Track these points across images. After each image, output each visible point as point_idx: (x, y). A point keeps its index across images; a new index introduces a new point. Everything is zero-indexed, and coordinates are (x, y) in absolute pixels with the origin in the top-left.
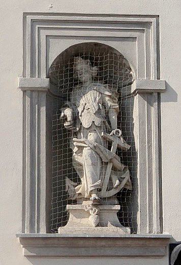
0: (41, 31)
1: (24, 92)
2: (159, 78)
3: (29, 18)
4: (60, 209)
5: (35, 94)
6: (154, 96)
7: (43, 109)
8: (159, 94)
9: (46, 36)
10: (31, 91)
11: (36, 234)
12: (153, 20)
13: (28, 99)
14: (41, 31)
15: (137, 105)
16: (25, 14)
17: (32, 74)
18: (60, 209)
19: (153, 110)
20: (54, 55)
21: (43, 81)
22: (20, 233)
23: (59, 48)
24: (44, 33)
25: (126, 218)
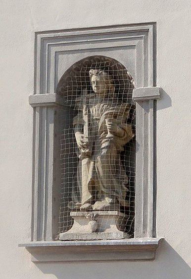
0: (60, 56)
1: (35, 108)
2: (155, 85)
3: (151, 27)
4: (66, 214)
5: (45, 110)
6: (154, 102)
7: (52, 127)
8: (155, 101)
9: (56, 52)
10: (40, 107)
11: (43, 242)
12: (151, 27)
13: (37, 114)
14: (60, 56)
15: (139, 110)
16: (36, 33)
17: (42, 92)
18: (66, 214)
19: (150, 114)
20: (63, 68)
21: (51, 96)
22: (28, 241)
23: (67, 62)
24: (54, 49)
25: (128, 228)
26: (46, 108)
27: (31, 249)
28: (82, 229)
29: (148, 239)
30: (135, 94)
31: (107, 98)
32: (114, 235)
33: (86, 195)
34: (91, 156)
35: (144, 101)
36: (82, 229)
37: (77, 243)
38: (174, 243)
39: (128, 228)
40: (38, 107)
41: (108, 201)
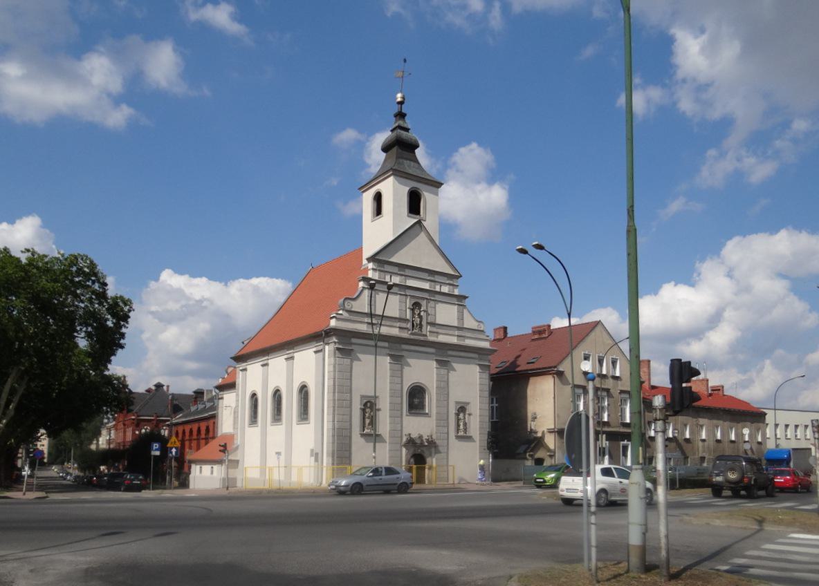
6: (379, 410)
28: (366, 431)
36: (366, 431)
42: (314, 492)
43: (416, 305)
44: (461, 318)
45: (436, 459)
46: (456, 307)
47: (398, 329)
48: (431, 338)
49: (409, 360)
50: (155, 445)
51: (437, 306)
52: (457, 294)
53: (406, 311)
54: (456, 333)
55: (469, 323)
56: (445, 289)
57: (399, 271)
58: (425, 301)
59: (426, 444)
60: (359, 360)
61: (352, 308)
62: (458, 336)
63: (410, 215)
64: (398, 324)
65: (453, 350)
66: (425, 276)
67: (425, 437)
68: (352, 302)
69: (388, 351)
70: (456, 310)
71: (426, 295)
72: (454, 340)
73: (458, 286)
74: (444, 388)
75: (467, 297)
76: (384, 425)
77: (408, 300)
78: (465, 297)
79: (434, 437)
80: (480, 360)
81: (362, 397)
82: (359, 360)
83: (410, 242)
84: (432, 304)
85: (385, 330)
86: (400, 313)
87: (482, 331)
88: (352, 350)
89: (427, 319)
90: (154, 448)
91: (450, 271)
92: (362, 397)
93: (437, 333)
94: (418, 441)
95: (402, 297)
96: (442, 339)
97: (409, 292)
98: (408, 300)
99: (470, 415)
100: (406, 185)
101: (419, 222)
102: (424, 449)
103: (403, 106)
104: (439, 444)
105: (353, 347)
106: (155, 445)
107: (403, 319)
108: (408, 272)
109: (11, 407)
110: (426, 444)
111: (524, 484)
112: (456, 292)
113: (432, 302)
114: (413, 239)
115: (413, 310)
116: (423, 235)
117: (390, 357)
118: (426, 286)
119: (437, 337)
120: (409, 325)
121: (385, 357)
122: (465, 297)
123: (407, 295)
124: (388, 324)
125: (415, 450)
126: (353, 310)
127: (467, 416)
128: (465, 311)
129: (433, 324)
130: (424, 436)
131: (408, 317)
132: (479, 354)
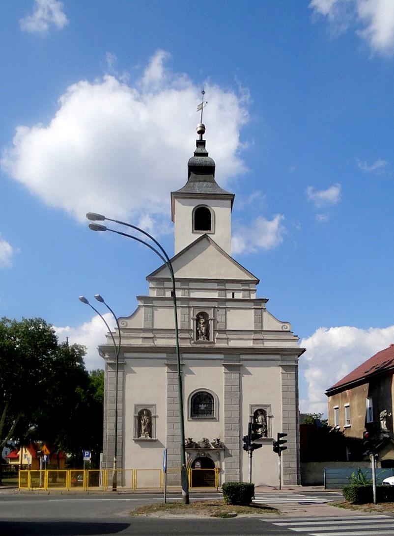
6: (155, 417)
15: (153, 418)
20: (254, 411)
21: (137, 415)
23: (140, 410)
25: (150, 436)
26: (192, 308)
27: (134, 440)
28: (143, 437)
29: (154, 439)
30: (152, 416)
31: (146, 415)
32: (149, 438)
33: (143, 431)
34: (144, 425)
35: (154, 417)
36: (143, 437)
37: (135, 346)
38: (159, 439)
39: (150, 436)
40: (135, 417)
41: (147, 432)
42: (75, 494)
43: (202, 316)
44: (259, 320)
45: (226, 463)
46: (253, 311)
47: (252, 341)
48: (218, 345)
49: (191, 368)
50: (86, 452)
51: (228, 312)
52: (255, 298)
53: (189, 321)
54: (253, 336)
55: (270, 323)
56: (239, 296)
57: (182, 285)
58: (192, 308)
59: (213, 448)
60: (192, 373)
61: (127, 325)
62: (254, 339)
63: (195, 231)
64: (141, 335)
65: (188, 353)
66: (215, 286)
67: (211, 441)
68: (127, 321)
69: (223, 362)
70: (253, 315)
71: (215, 304)
72: (250, 344)
73: (256, 290)
74: (236, 394)
75: (268, 300)
76: (162, 429)
77: (192, 312)
78: (266, 301)
79: (222, 440)
80: (282, 360)
81: (136, 406)
82: (192, 373)
83: (195, 257)
84: (222, 312)
85: (160, 343)
86: (256, 326)
87: (289, 331)
88: (241, 365)
89: (214, 327)
90: (86, 455)
91: (247, 277)
92: (136, 406)
93: (228, 339)
94: (203, 446)
95: (184, 309)
96: (233, 344)
97: (192, 304)
98: (192, 312)
99: (270, 417)
100: (190, 205)
101: (205, 236)
102: (210, 452)
103: (203, 135)
104: (228, 448)
105: (126, 361)
106: (86, 452)
107: (222, 331)
108: (192, 285)
109: (12, 428)
110: (213, 448)
111: (326, 488)
112: (253, 296)
113: (220, 310)
114: (200, 253)
115: (198, 320)
116: (211, 248)
117: (225, 367)
118: (215, 295)
119: (263, 344)
120: (193, 335)
121: (162, 368)
122: (266, 301)
123: (190, 307)
124: (166, 336)
125: (198, 454)
126: (127, 327)
127: (268, 418)
128: (265, 314)
129: (224, 331)
130: (210, 440)
131: (192, 328)
132: (282, 355)
